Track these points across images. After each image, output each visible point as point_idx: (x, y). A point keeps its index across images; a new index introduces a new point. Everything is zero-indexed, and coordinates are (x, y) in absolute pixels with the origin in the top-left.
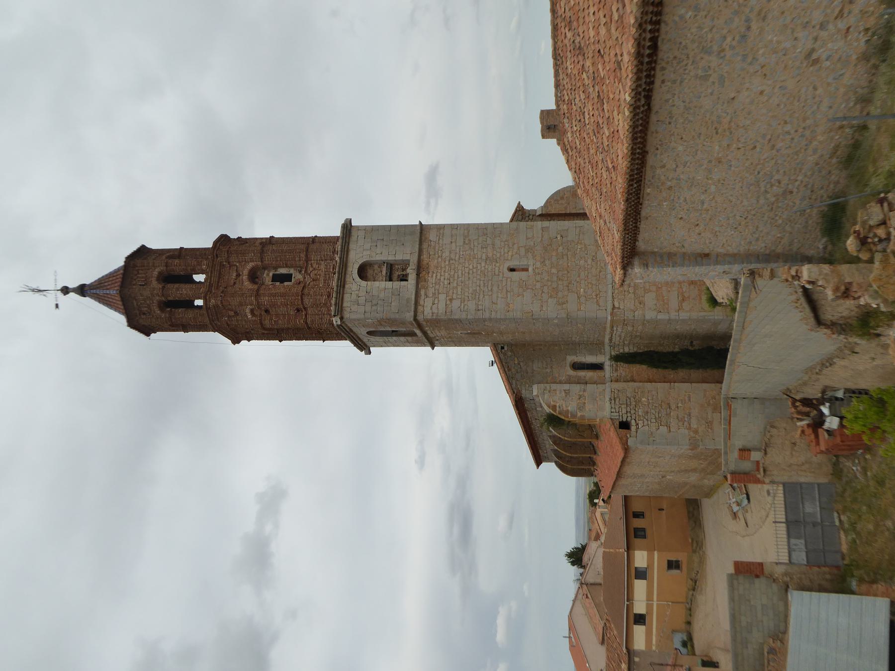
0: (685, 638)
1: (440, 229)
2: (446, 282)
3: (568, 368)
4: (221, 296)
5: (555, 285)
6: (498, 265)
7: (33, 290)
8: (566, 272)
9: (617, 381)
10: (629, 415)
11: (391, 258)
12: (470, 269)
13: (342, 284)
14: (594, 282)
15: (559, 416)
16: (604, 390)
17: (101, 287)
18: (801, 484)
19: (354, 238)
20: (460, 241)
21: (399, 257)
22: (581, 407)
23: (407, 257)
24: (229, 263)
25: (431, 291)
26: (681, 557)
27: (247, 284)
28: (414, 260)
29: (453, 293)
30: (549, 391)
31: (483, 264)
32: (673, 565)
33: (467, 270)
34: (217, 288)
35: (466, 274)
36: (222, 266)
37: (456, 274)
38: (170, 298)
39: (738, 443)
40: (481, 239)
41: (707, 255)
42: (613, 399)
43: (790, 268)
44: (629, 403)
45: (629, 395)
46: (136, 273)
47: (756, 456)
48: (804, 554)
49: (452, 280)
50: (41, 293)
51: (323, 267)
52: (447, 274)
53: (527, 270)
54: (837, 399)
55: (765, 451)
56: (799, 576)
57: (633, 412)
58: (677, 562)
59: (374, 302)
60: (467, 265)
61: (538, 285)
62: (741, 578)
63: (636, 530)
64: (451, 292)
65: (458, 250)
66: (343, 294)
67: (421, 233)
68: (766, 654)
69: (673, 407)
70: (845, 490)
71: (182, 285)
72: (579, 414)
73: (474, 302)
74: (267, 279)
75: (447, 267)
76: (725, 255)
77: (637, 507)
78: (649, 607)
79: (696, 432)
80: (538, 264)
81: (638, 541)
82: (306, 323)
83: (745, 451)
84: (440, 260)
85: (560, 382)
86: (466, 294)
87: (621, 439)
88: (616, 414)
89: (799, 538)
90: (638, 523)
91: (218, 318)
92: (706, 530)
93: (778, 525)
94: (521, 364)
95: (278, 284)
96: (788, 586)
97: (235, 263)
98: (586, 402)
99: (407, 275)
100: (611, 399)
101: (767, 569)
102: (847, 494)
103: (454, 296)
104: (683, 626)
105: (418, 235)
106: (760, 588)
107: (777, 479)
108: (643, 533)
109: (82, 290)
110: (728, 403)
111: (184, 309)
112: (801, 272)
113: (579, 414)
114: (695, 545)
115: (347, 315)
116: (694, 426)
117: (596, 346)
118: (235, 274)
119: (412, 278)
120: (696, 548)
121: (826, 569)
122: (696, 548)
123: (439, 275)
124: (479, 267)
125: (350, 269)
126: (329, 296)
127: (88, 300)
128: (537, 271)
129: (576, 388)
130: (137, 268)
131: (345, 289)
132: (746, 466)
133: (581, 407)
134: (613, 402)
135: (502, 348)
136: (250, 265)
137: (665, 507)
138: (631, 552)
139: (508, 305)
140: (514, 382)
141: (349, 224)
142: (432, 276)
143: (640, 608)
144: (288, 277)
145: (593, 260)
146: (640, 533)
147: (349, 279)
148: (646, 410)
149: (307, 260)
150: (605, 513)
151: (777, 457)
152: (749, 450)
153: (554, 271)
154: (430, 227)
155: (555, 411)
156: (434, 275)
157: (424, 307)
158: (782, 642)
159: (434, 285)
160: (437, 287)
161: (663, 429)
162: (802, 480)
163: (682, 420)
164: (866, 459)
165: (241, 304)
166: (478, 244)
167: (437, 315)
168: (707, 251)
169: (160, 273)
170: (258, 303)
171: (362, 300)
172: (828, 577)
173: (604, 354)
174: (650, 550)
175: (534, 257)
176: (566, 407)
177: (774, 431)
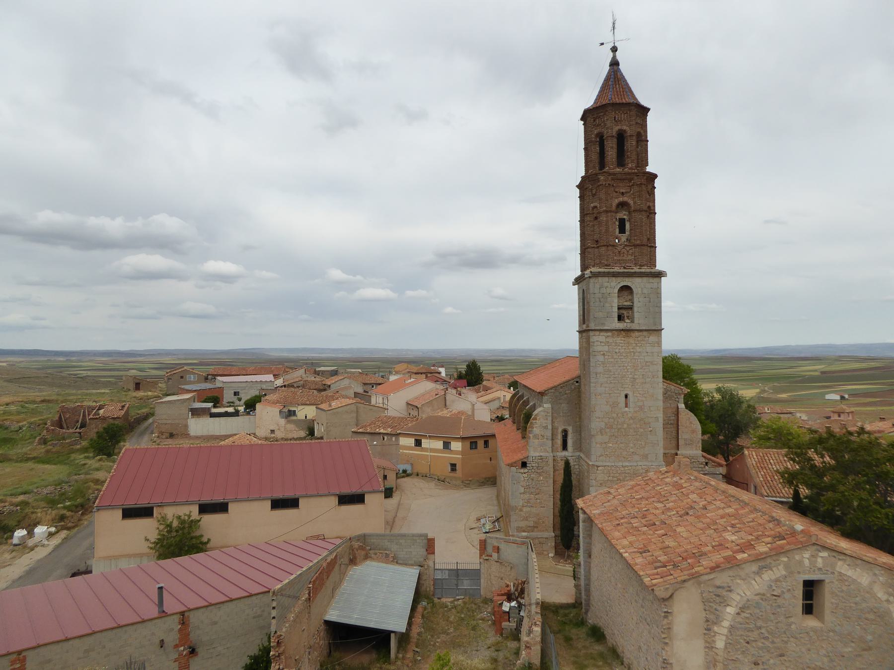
0: (408, 472)
1: (658, 344)
2: (617, 350)
3: (563, 427)
4: (606, 184)
5: (614, 426)
6: (630, 387)
7: (614, 24)
8: (624, 434)
9: (554, 460)
10: (531, 468)
11: (635, 309)
12: (626, 367)
13: (615, 275)
14: (616, 453)
15: (529, 423)
16: (548, 452)
17: (615, 82)
18: (480, 579)
19: (651, 280)
20: (647, 359)
21: (636, 315)
22: (536, 437)
23: (636, 321)
24: (633, 185)
25: (610, 340)
26: (459, 472)
27: (616, 201)
28: (634, 326)
29: (609, 356)
30: (546, 416)
31: (630, 376)
32: (453, 467)
33: (626, 365)
34: (612, 179)
35: (623, 365)
36: (630, 180)
37: (622, 357)
38: (605, 141)
39: (502, 546)
40: (650, 374)
41: (590, 556)
42: (541, 458)
43: (540, 621)
44: (539, 468)
45: (544, 468)
46: (625, 112)
47: (495, 555)
48: (440, 578)
49: (618, 354)
50: (612, 29)
51: (630, 257)
52: (623, 350)
53: (626, 406)
54: (520, 611)
55: (498, 562)
56: (428, 573)
57: (533, 470)
58: (456, 470)
59: (602, 300)
60: (630, 364)
61: (614, 415)
62: (426, 541)
63: (476, 442)
64: (610, 354)
65: (642, 357)
66: (608, 276)
67: (655, 330)
68: (386, 552)
69: (537, 497)
70: (475, 604)
71: (615, 150)
72: (531, 435)
73: (602, 371)
74: (621, 214)
75: (628, 351)
76: (590, 567)
77: (491, 442)
78: (426, 450)
79: (521, 510)
80: (630, 415)
81: (468, 444)
82: (588, 248)
83: (498, 550)
84: (635, 345)
85: (553, 422)
86: (608, 365)
87: (515, 463)
88: (531, 459)
89: (449, 576)
90: (481, 443)
91: (590, 181)
92: (477, 490)
93: (456, 564)
94: (566, 395)
95: (617, 223)
96: (422, 567)
97: (632, 190)
98: (539, 440)
99: (624, 320)
100: (541, 456)
101: (431, 556)
102: (473, 606)
103: (606, 357)
104: (415, 471)
105: (653, 328)
106: (419, 551)
107: (482, 566)
108: (474, 447)
109: (615, 64)
110: (525, 544)
111: (598, 151)
112: (538, 627)
113: (531, 435)
114: (467, 482)
115: (592, 280)
116: (525, 509)
117: (579, 447)
118: (624, 191)
119: (621, 325)
120: (465, 483)
121: (432, 588)
122: (465, 483)
123: (623, 345)
124: (628, 373)
125: (627, 279)
126: (606, 265)
127: (606, 68)
128: (625, 414)
129: (549, 433)
130: (628, 112)
131: (612, 278)
132: (489, 549)
133: (536, 437)
134: (540, 458)
135: (577, 382)
136: (631, 202)
137: (492, 462)
138: (461, 440)
139: (600, 394)
140: (553, 391)
141: (661, 276)
142: (621, 340)
143: (425, 443)
144: (622, 230)
145: (633, 453)
146: (473, 445)
147: (619, 279)
148: (534, 479)
149: (635, 246)
150: (500, 401)
151: (495, 567)
152: (498, 552)
153: (625, 426)
154: (660, 336)
155: (533, 420)
156: (623, 342)
157: (599, 335)
158: (392, 561)
159: (615, 342)
160: (613, 344)
161: (522, 490)
162: (482, 581)
163: (528, 502)
164: (488, 621)
165: (600, 199)
166: (646, 372)
167: (592, 345)
168: (592, 557)
169: (625, 131)
170: (601, 213)
171: (603, 290)
172: (428, 589)
173: (573, 452)
174: (462, 453)
175: (636, 412)
176: (536, 427)
177: (509, 568)
